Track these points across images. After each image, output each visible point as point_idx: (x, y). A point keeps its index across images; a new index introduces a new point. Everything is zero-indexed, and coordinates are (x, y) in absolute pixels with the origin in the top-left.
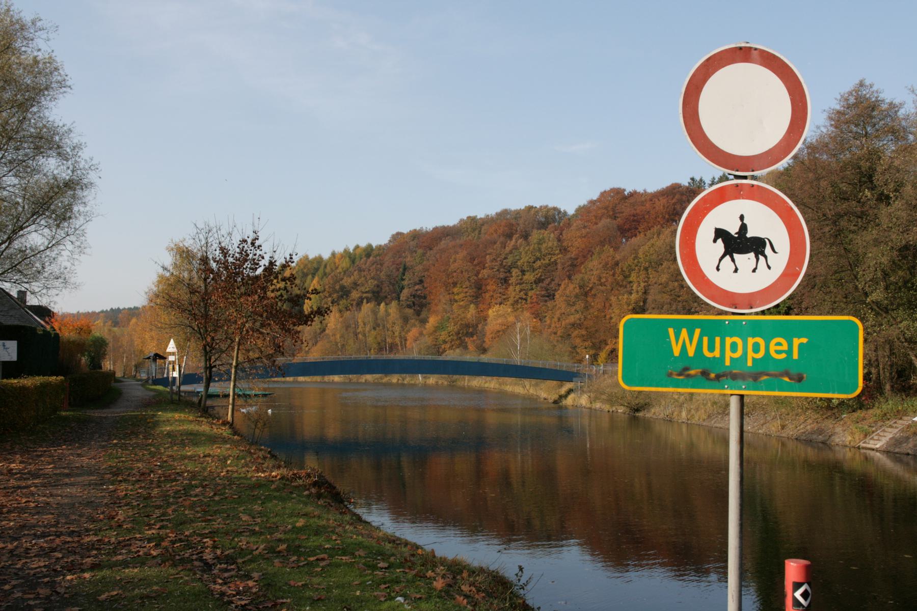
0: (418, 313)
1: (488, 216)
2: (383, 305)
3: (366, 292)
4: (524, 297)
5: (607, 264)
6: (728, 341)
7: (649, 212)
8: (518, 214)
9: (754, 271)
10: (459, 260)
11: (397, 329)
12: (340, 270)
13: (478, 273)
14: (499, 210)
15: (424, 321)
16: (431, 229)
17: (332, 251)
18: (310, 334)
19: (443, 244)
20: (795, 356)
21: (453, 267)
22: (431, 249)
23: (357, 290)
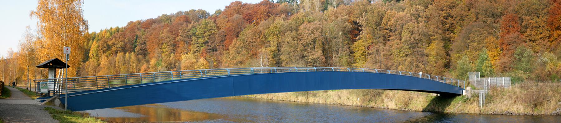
0: (145, 57)
2: (127, 54)
3: (119, 48)
4: (199, 50)
5: (255, 32)
7: (256, 12)
10: (164, 33)
11: (135, 65)
12: (105, 37)
13: (175, 38)
15: (148, 62)
17: (101, 29)
18: (92, 67)
19: (154, 26)
21: (162, 36)
22: (148, 28)
23: (115, 47)
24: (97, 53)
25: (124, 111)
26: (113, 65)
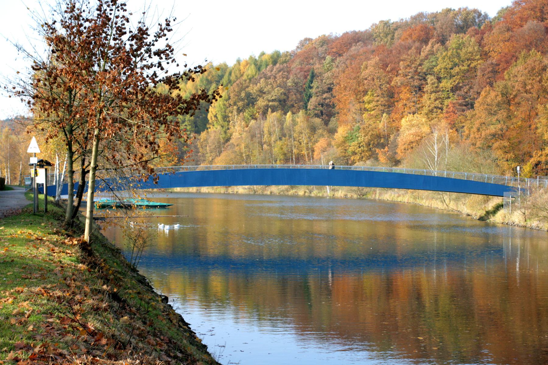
2: (289, 114)
3: (273, 101)
12: (245, 77)
15: (332, 131)
21: (365, 73)
24: (225, 112)
25: (334, 343)
26: (257, 140)
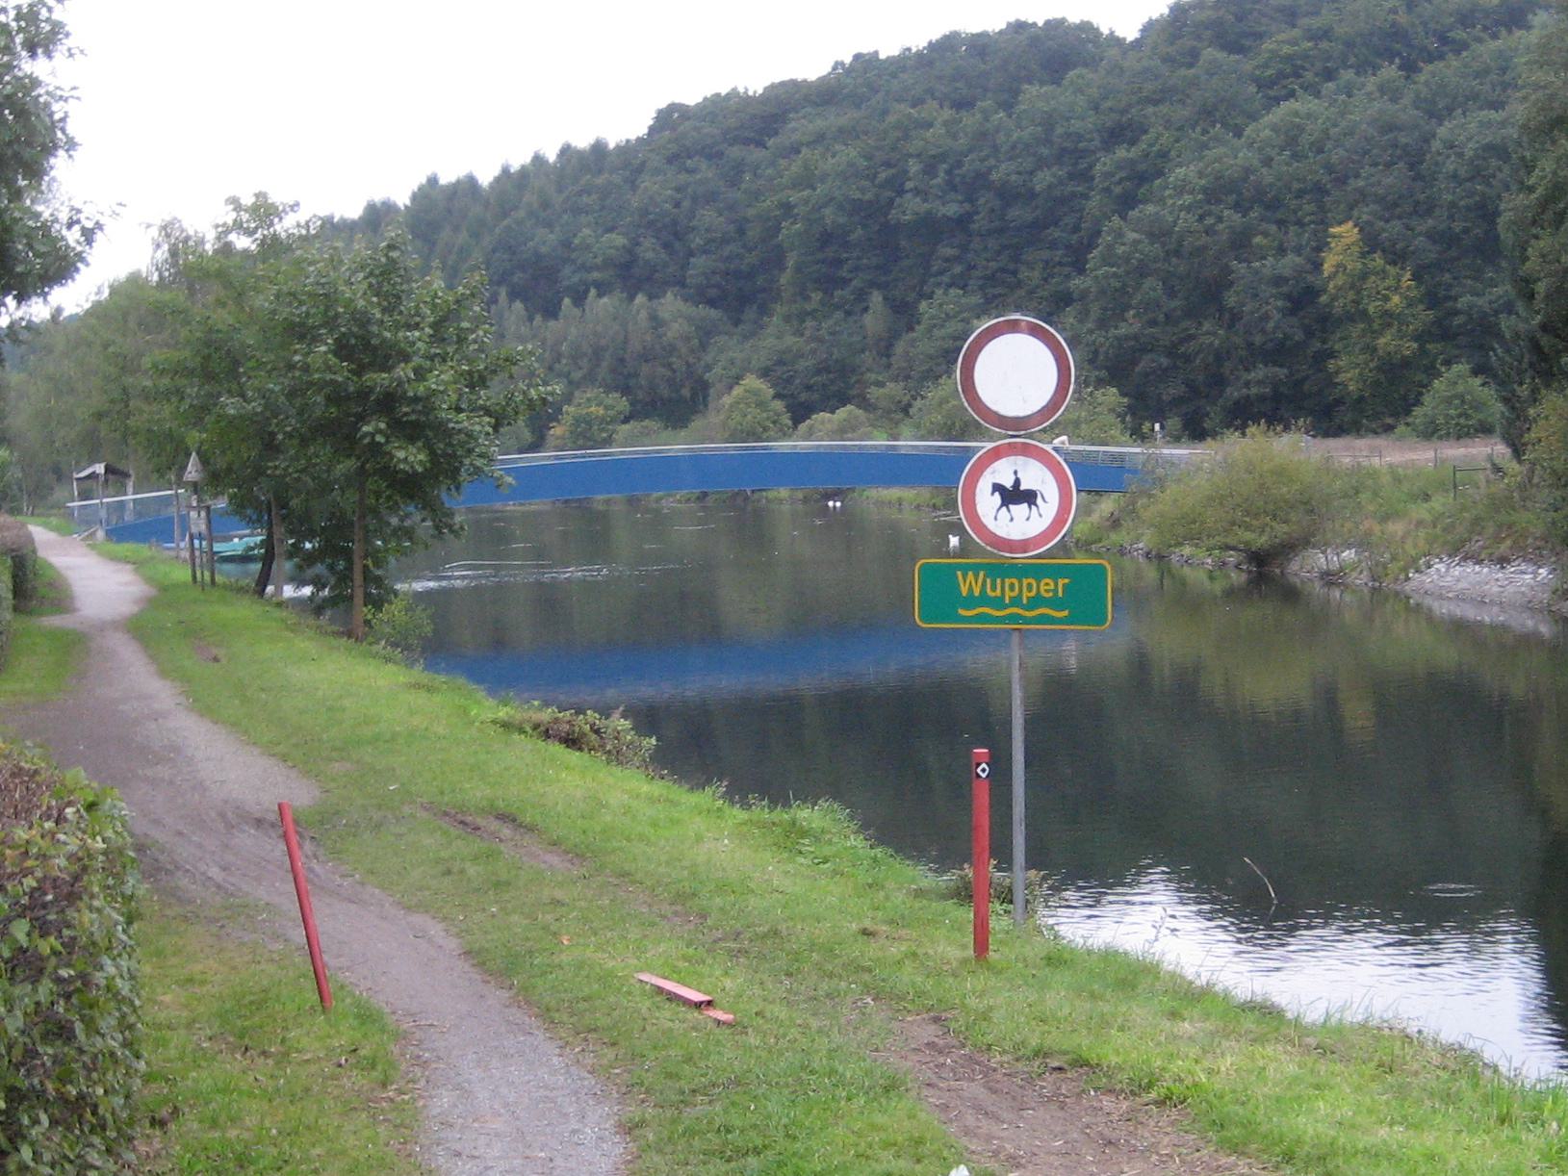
1: (909, 49)
2: (640, 299)
4: (1011, 266)
6: (1007, 581)
8: (980, 45)
9: (1028, 519)
14: (936, 35)
16: (760, 91)
17: (504, 161)
20: (1060, 594)
